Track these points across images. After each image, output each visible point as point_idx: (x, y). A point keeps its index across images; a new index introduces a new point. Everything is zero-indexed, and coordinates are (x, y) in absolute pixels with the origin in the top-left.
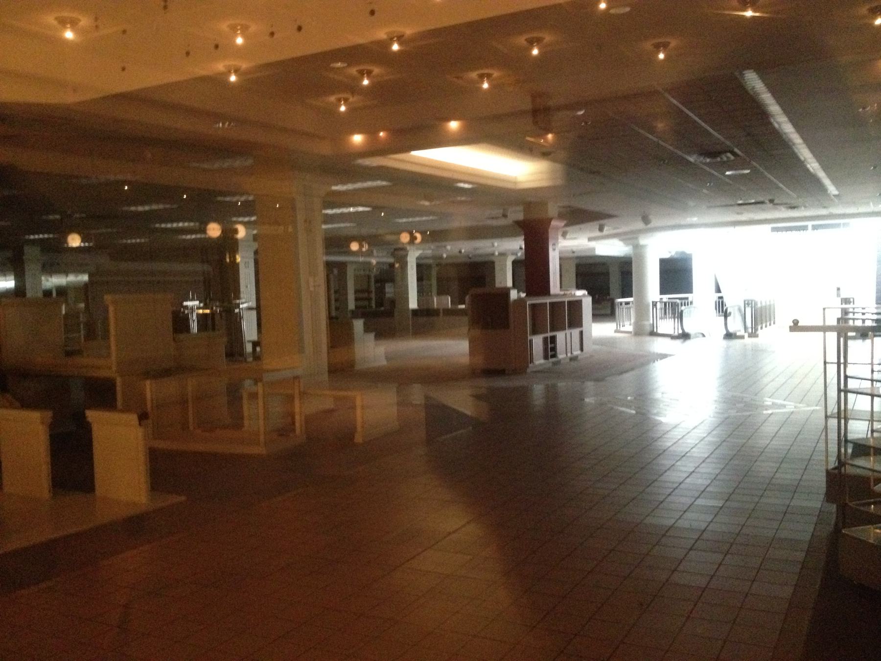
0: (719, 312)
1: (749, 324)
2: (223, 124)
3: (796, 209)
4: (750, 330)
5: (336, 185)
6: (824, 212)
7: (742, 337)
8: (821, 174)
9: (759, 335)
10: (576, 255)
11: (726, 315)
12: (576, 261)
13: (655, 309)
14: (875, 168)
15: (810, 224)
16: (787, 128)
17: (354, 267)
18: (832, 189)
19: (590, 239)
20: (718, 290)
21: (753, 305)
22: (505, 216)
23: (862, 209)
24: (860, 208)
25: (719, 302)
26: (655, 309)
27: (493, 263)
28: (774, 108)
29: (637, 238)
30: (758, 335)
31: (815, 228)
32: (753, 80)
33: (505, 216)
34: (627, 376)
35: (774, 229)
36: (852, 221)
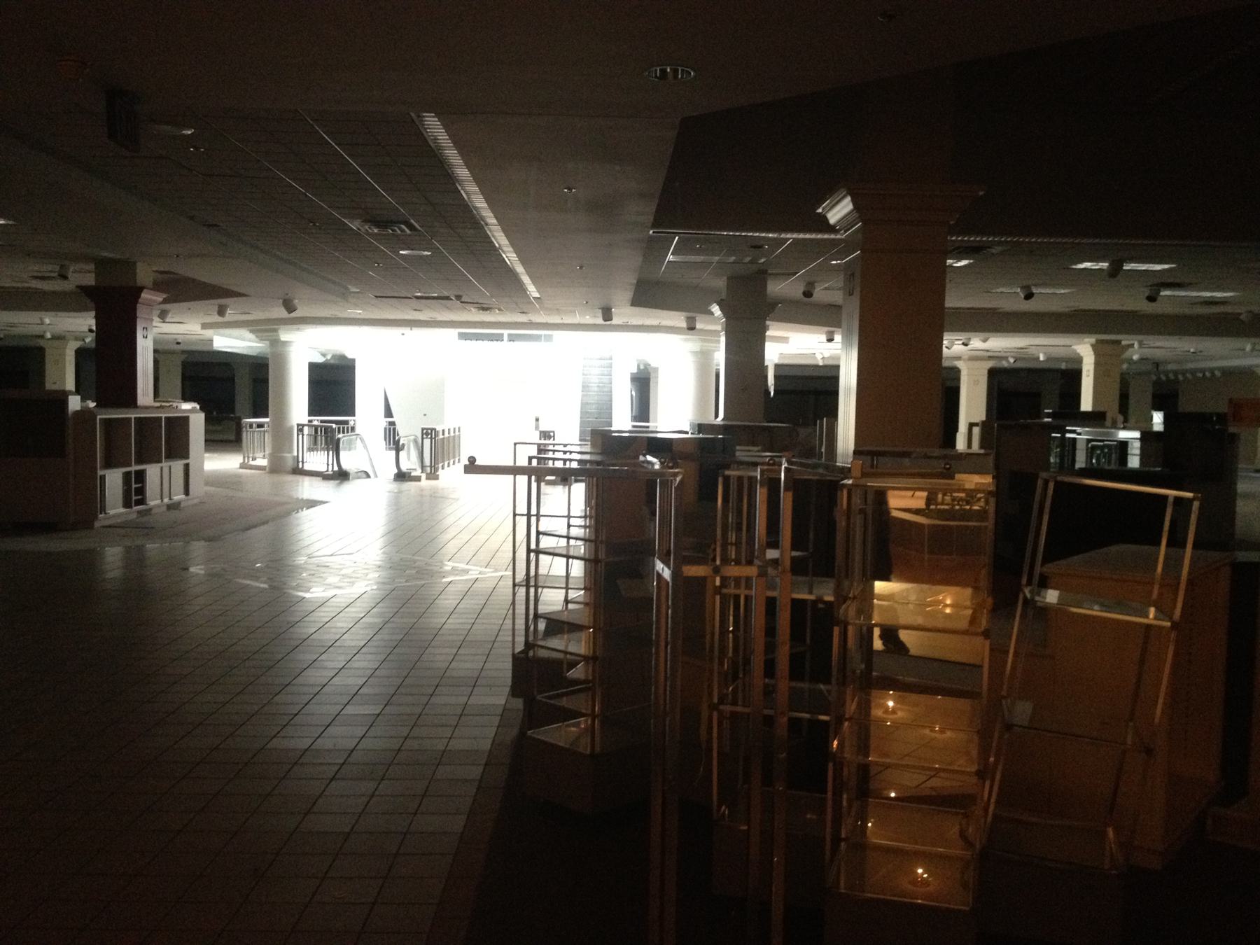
0: (390, 444)
1: (427, 461)
4: (428, 470)
7: (418, 479)
9: (440, 477)
11: (397, 447)
12: (183, 357)
13: (300, 436)
15: (506, 332)
16: (479, 202)
18: (533, 291)
19: (205, 326)
20: (389, 413)
21: (433, 437)
22: (64, 277)
23: (568, 320)
25: (390, 429)
26: (300, 436)
27: (41, 350)
28: (462, 172)
29: (275, 331)
30: (438, 475)
31: (512, 338)
32: (434, 127)
33: (64, 277)
35: (463, 337)
36: (557, 334)
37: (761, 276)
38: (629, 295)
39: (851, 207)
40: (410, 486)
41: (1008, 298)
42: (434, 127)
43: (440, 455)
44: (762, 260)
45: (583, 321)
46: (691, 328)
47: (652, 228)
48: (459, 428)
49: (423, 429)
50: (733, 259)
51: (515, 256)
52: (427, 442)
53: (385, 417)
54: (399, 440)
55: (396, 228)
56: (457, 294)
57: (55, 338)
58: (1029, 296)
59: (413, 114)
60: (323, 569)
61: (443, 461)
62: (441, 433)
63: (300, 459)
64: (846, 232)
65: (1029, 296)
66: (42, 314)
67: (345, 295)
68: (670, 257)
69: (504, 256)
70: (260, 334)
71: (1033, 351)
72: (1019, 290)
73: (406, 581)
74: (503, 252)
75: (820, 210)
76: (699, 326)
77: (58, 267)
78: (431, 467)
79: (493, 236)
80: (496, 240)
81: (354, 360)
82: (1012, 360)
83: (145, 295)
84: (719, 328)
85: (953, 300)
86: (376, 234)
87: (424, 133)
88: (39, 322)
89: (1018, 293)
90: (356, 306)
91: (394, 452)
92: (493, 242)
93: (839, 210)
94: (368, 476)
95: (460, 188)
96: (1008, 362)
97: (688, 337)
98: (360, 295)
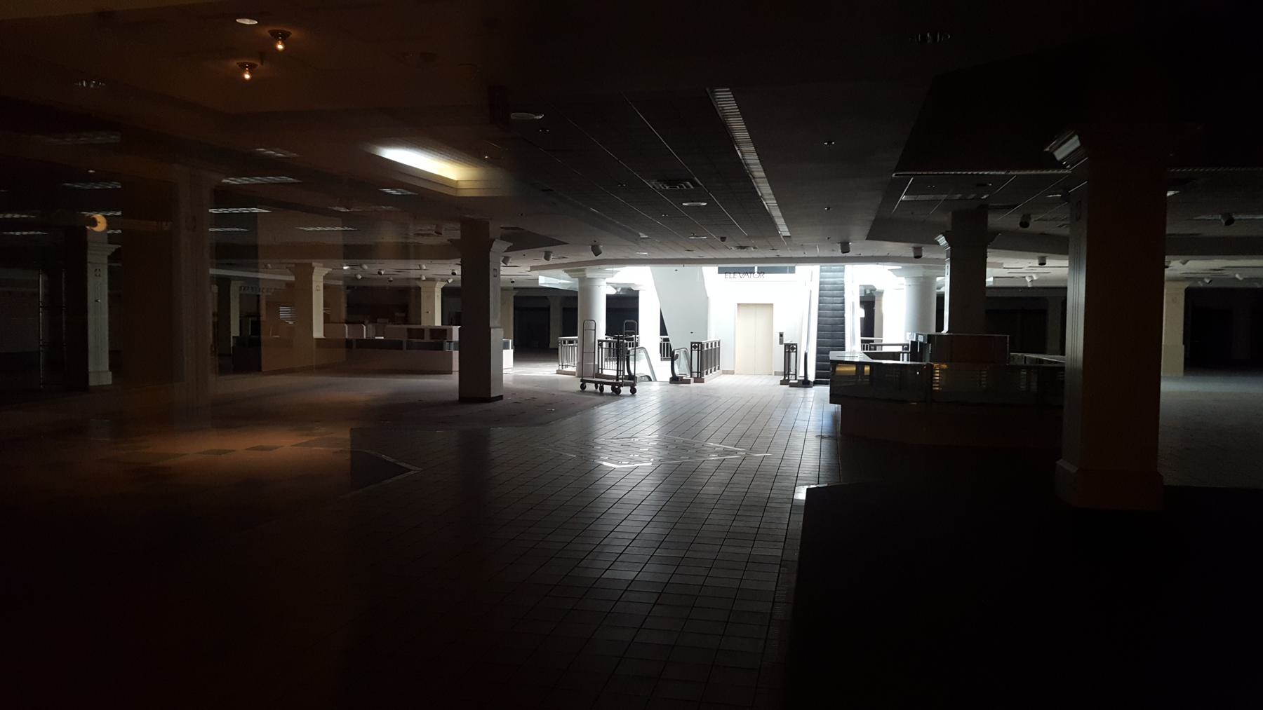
0: (664, 356)
1: (695, 369)
2: (88, 84)
3: (745, 250)
4: (695, 375)
5: (227, 177)
6: (772, 254)
8: (776, 213)
10: (513, 285)
12: (515, 293)
13: (600, 349)
14: (828, 209)
16: (752, 159)
17: (240, 283)
18: (784, 230)
19: (533, 268)
20: (663, 331)
22: (439, 233)
24: (1049, 263)
26: (600, 349)
28: (741, 134)
29: (583, 270)
31: (761, 271)
32: (726, 101)
33: (439, 233)
34: (570, 420)
35: (721, 271)
37: (983, 210)
38: (867, 230)
39: (1078, 144)
40: (682, 387)
41: (1210, 225)
42: (726, 101)
43: (705, 366)
44: (985, 197)
45: (822, 255)
46: (918, 257)
47: (894, 172)
48: (719, 343)
49: (692, 343)
50: (959, 196)
51: (775, 202)
52: (695, 353)
53: (661, 335)
54: (674, 352)
55: (683, 185)
56: (722, 236)
57: (427, 279)
58: (1230, 222)
59: (707, 89)
60: (626, 448)
61: (707, 368)
62: (705, 346)
63: (600, 367)
64: (1072, 166)
65: (1230, 222)
66: (421, 262)
67: (637, 240)
68: (903, 197)
69: (764, 203)
70: (572, 273)
71: (1229, 273)
72: (1220, 217)
73: (690, 458)
74: (765, 200)
75: (1047, 149)
76: (924, 255)
77: (435, 226)
78: (698, 372)
79: (758, 187)
80: (759, 189)
81: (637, 292)
82: (1208, 281)
83: (495, 245)
84: (944, 256)
85: (1173, 228)
86: (667, 190)
87: (715, 105)
88: (419, 268)
89: (1220, 220)
90: (644, 250)
91: (669, 363)
92: (757, 192)
93: (1066, 149)
94: (650, 380)
95: (737, 149)
96: (1204, 282)
97: (911, 265)
98: (648, 240)
